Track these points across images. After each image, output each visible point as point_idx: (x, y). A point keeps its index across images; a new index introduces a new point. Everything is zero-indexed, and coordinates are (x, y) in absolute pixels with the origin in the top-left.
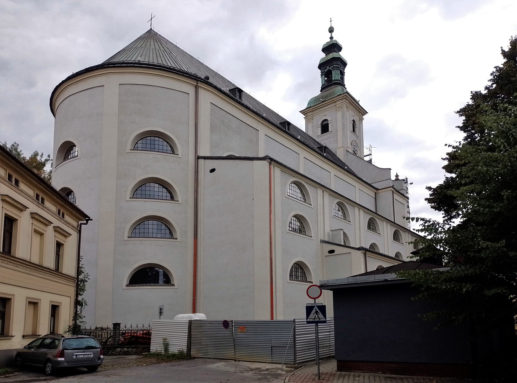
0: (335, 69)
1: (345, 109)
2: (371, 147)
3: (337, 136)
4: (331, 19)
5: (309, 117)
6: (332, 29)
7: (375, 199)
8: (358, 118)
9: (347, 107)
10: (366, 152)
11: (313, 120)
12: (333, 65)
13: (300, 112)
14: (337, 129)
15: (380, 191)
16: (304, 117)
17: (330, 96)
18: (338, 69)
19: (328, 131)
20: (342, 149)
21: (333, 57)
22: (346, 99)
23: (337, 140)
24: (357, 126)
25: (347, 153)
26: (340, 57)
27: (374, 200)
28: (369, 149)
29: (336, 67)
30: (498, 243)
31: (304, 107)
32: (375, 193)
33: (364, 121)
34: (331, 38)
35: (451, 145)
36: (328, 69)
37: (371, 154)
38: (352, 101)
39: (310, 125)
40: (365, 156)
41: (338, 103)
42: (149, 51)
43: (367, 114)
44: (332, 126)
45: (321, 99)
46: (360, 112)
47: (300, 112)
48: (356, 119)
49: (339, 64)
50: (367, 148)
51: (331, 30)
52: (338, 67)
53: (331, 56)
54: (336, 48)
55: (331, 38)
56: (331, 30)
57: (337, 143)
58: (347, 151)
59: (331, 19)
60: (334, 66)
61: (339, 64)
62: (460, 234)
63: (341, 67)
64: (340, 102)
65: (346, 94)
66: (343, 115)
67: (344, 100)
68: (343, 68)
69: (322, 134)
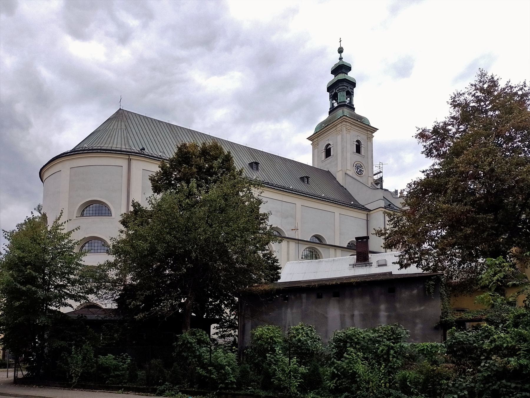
0: (340, 92)
1: (345, 132)
2: (381, 164)
3: (337, 159)
4: (340, 39)
5: (315, 143)
6: (340, 50)
7: (367, 220)
8: (365, 137)
9: (347, 130)
10: (376, 170)
11: (319, 145)
12: (338, 87)
13: (307, 139)
14: (337, 152)
15: (371, 212)
16: (311, 142)
17: (332, 120)
18: (344, 91)
19: (330, 155)
20: (341, 172)
21: (338, 80)
22: (346, 122)
23: (337, 163)
24: (363, 146)
25: (346, 176)
26: (345, 79)
27: (366, 221)
28: (379, 167)
29: (341, 89)
30: (172, 368)
31: (311, 132)
32: (367, 214)
33: (374, 139)
34: (341, 59)
35: (425, 170)
36: (334, 92)
37: (381, 172)
38: (353, 122)
39: (316, 150)
40: (375, 175)
41: (338, 126)
42: (130, 121)
43: (378, 131)
44: (333, 149)
45: (323, 125)
46: (367, 131)
47: (307, 139)
48: (362, 138)
49: (344, 86)
50: (376, 166)
51: (341, 51)
52: (344, 89)
53: (341, 76)
54: (344, 68)
55: (341, 59)
56: (341, 51)
57: (337, 166)
58: (345, 173)
59: (340, 39)
60: (340, 88)
61: (344, 86)
62: (93, 361)
63: (348, 87)
64: (340, 125)
65: (344, 117)
66: (342, 138)
67: (344, 123)
68: (350, 88)
69: (326, 158)
